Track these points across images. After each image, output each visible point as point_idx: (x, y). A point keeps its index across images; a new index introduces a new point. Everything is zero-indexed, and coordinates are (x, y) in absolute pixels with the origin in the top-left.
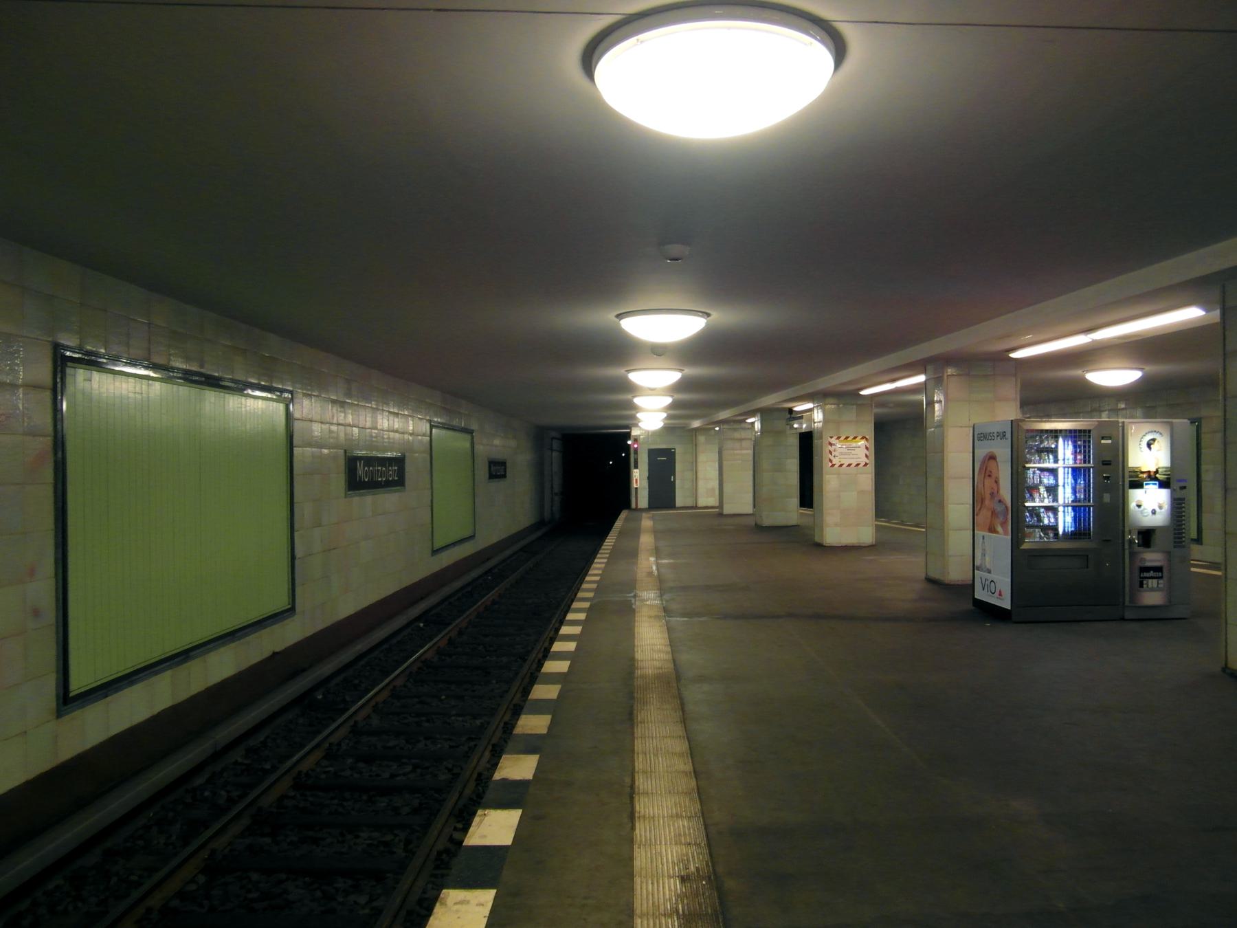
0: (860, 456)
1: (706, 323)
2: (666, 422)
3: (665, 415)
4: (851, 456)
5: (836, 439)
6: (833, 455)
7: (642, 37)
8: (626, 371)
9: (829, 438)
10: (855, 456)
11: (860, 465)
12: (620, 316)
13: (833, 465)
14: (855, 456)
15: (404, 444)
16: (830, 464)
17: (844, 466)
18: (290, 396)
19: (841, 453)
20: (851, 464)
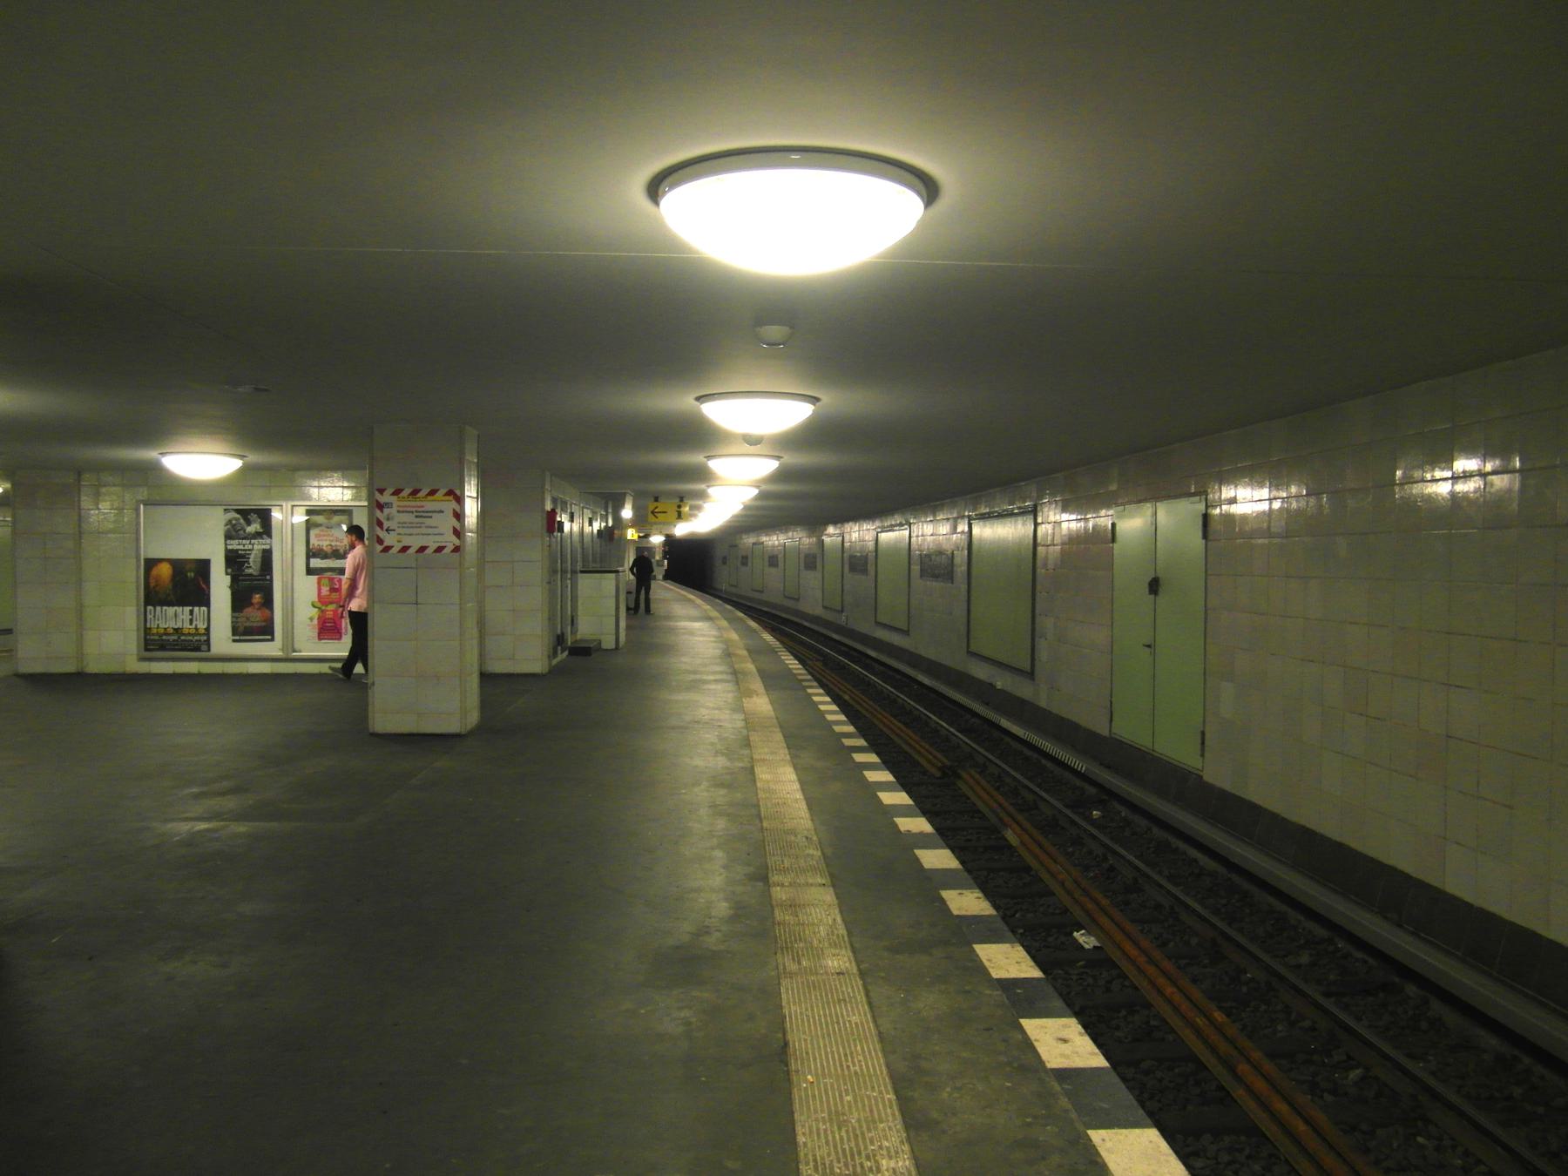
0: (441, 531)
1: (814, 411)
2: (764, 487)
3: (755, 492)
4: (424, 530)
5: (393, 494)
6: (385, 527)
7: (720, 176)
8: (705, 457)
9: (377, 494)
10: (430, 531)
11: (445, 551)
12: (655, 189)
13: (387, 549)
14: (430, 531)
15: (1409, 498)
16: (380, 548)
17: (411, 551)
18: (1193, 491)
19: (403, 524)
20: (409, 547)
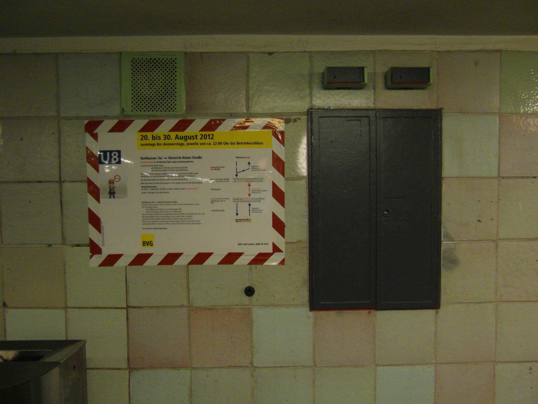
20: (274, 217)
